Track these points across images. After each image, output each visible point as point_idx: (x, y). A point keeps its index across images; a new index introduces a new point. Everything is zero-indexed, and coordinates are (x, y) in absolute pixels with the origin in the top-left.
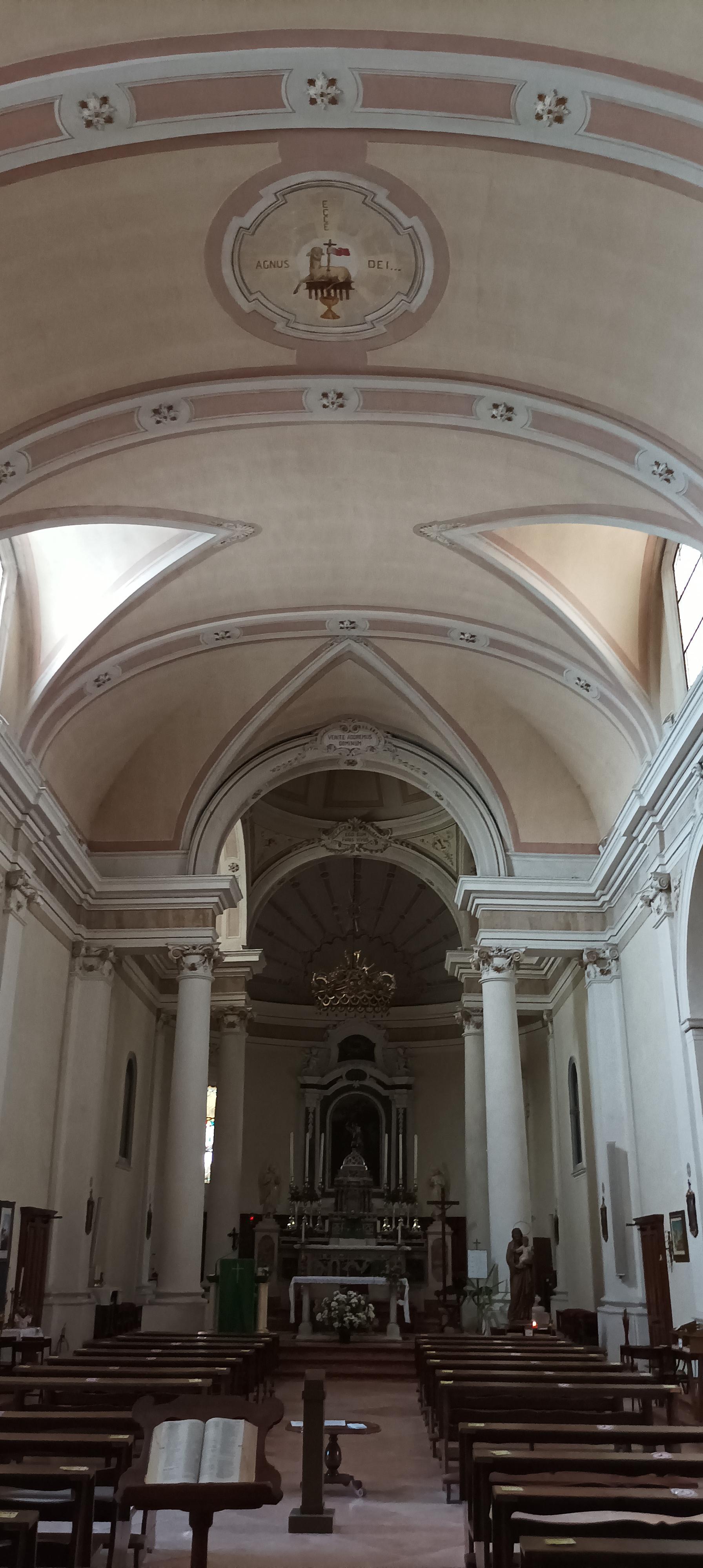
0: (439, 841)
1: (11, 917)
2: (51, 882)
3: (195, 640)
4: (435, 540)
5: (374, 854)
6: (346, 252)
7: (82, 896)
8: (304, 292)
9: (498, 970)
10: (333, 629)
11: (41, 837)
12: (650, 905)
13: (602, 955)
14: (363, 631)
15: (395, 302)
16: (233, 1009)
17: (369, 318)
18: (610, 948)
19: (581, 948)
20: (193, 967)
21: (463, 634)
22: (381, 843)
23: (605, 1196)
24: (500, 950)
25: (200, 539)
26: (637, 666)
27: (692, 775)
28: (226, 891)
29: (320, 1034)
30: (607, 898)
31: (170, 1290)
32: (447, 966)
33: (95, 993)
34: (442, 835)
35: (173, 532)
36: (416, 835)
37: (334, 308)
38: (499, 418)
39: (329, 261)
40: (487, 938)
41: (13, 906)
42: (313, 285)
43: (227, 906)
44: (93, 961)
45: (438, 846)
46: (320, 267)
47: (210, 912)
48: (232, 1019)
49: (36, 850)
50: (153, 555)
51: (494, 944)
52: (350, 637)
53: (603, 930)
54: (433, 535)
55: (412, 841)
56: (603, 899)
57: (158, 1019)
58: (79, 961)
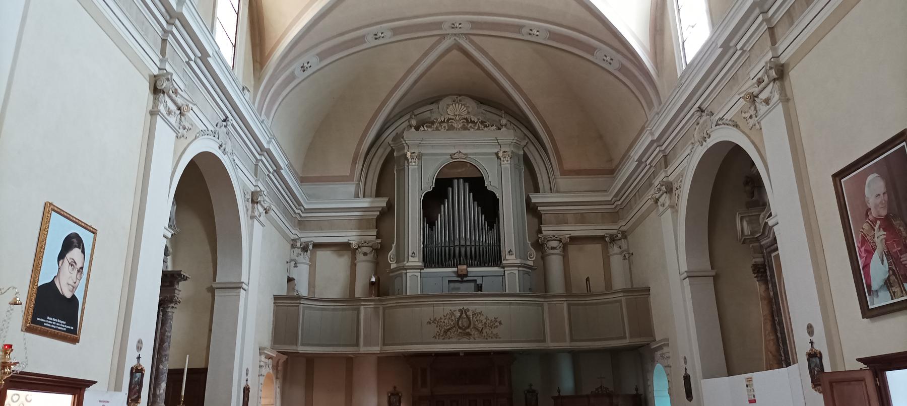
10: (446, 29)
11: (193, 57)
30: (619, 203)
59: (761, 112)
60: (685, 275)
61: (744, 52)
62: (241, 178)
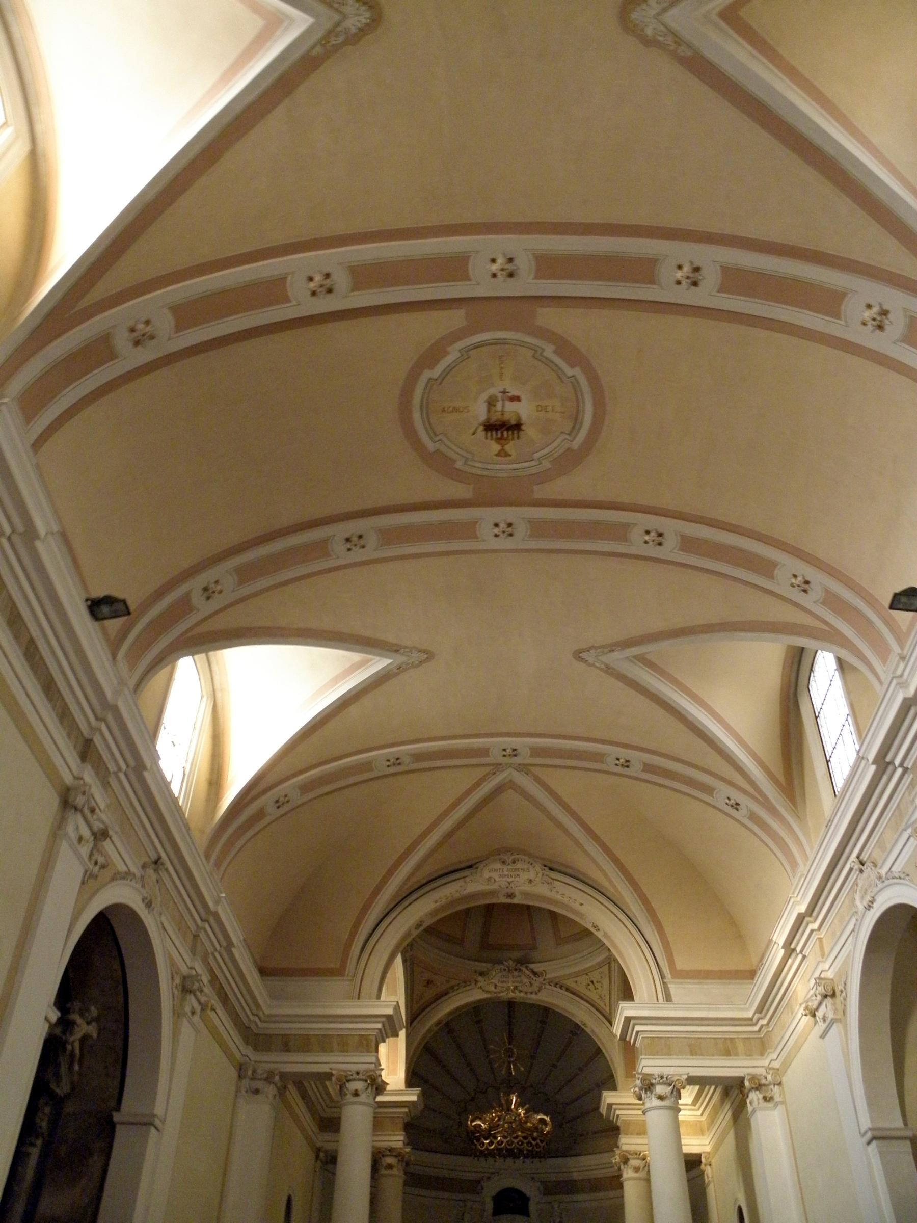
0: (592, 982)
1: (185, 1021)
2: (224, 999)
3: (367, 766)
4: (593, 665)
5: (529, 996)
6: (517, 399)
8: (481, 433)
9: (661, 1098)
10: (495, 757)
12: (814, 1015)
13: (763, 1081)
14: (525, 758)
15: (559, 441)
16: (391, 1150)
17: (536, 455)
18: (771, 1072)
19: (742, 1075)
20: (356, 1094)
21: (618, 759)
22: (536, 985)
24: (662, 1077)
25: (378, 664)
26: (782, 779)
27: (851, 870)
28: (389, 1017)
29: (474, 1187)
30: (764, 1022)
32: (603, 1110)
33: (257, 1116)
34: (595, 976)
35: (355, 657)
36: (570, 976)
37: (507, 448)
38: (651, 543)
39: (503, 406)
40: (649, 1065)
41: (188, 1009)
42: (490, 427)
43: (390, 1034)
44: (259, 1085)
45: (591, 986)
46: (496, 411)
47: (374, 1038)
48: (390, 1160)
49: (211, 960)
50: (336, 680)
51: (656, 1071)
52: (510, 765)
53: (762, 1054)
54: (591, 660)
55: (565, 982)
57: (317, 1157)
58: (245, 1083)
62: (169, 951)
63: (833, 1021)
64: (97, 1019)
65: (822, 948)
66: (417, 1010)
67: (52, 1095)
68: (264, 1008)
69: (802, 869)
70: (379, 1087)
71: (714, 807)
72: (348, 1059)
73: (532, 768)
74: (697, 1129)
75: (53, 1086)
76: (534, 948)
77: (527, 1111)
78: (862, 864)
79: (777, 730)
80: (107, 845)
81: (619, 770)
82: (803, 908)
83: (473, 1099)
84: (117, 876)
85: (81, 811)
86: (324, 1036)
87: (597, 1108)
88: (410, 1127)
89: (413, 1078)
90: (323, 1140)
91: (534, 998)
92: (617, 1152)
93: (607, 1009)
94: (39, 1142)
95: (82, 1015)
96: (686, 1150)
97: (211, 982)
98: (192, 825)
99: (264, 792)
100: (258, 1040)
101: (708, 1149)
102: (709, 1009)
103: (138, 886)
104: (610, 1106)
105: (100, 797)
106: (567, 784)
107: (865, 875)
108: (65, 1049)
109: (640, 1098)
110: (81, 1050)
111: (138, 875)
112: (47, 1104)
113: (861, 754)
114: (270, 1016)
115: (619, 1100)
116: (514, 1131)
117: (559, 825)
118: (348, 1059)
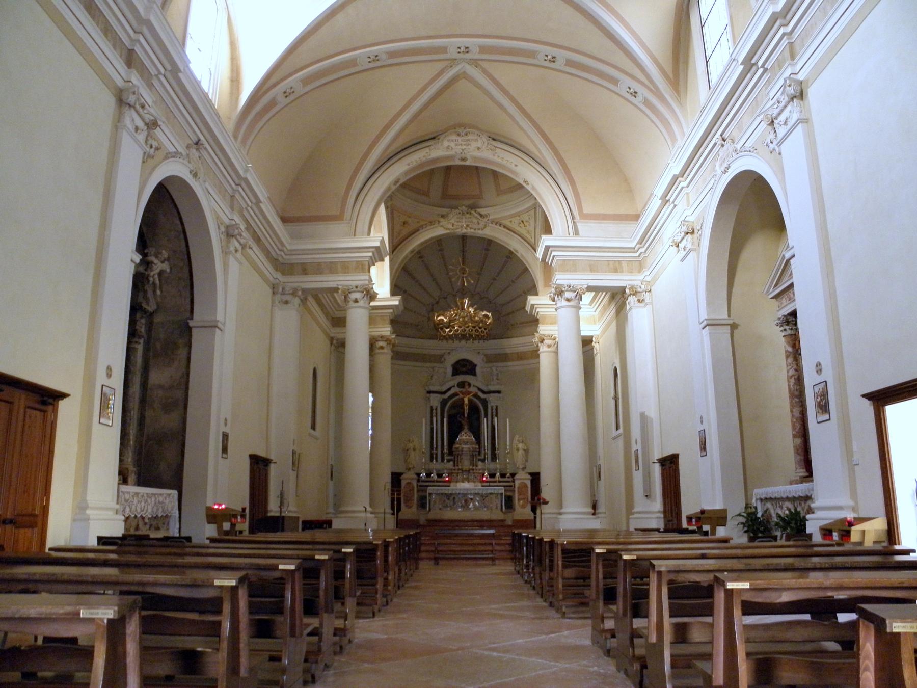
2: (258, 240)
3: (353, 62)
7: (279, 252)
9: (568, 300)
10: (453, 53)
11: (162, 71)
12: (678, 246)
13: (639, 290)
14: (475, 54)
20: (356, 301)
22: (481, 226)
23: (636, 446)
26: (671, 76)
27: (715, 144)
28: (377, 248)
29: (440, 359)
30: (643, 250)
31: (350, 508)
32: (528, 308)
33: (288, 319)
34: (525, 217)
36: (505, 218)
40: (561, 278)
41: (232, 249)
45: (522, 225)
48: (381, 344)
49: (246, 213)
51: (565, 283)
52: (464, 60)
56: (641, 250)
57: (331, 344)
58: (278, 297)
59: (780, 135)
60: (705, 323)
61: (766, 70)
62: (213, 207)
63: (690, 251)
64: (168, 259)
65: (688, 200)
66: (396, 244)
67: (145, 311)
68: (287, 245)
69: (680, 142)
70: (372, 296)
71: (618, 94)
72: (348, 278)
73: (480, 62)
74: (593, 320)
75: (144, 306)
76: (480, 197)
77: (476, 310)
78: (724, 140)
79: (670, 36)
80: (158, 131)
81: (547, 64)
82: (677, 170)
83: (437, 303)
84: (169, 156)
85: (134, 107)
86: (331, 263)
87: (524, 308)
88: (394, 322)
89: (396, 289)
90: (335, 332)
91: (480, 233)
92: (537, 335)
93: (533, 240)
94: (142, 341)
95: (156, 257)
96: (583, 333)
97: (247, 229)
98: (221, 114)
99: (274, 85)
100: (284, 267)
101: (598, 333)
102: (605, 241)
103: (186, 162)
104: (533, 306)
105: (147, 96)
106: (508, 74)
107: (724, 148)
108: (149, 281)
109: (554, 300)
110: (160, 280)
111: (184, 153)
112: (142, 318)
113: (733, 56)
114: (291, 250)
115: (540, 302)
116: (466, 323)
117: (501, 106)
118: (348, 278)
